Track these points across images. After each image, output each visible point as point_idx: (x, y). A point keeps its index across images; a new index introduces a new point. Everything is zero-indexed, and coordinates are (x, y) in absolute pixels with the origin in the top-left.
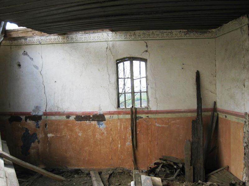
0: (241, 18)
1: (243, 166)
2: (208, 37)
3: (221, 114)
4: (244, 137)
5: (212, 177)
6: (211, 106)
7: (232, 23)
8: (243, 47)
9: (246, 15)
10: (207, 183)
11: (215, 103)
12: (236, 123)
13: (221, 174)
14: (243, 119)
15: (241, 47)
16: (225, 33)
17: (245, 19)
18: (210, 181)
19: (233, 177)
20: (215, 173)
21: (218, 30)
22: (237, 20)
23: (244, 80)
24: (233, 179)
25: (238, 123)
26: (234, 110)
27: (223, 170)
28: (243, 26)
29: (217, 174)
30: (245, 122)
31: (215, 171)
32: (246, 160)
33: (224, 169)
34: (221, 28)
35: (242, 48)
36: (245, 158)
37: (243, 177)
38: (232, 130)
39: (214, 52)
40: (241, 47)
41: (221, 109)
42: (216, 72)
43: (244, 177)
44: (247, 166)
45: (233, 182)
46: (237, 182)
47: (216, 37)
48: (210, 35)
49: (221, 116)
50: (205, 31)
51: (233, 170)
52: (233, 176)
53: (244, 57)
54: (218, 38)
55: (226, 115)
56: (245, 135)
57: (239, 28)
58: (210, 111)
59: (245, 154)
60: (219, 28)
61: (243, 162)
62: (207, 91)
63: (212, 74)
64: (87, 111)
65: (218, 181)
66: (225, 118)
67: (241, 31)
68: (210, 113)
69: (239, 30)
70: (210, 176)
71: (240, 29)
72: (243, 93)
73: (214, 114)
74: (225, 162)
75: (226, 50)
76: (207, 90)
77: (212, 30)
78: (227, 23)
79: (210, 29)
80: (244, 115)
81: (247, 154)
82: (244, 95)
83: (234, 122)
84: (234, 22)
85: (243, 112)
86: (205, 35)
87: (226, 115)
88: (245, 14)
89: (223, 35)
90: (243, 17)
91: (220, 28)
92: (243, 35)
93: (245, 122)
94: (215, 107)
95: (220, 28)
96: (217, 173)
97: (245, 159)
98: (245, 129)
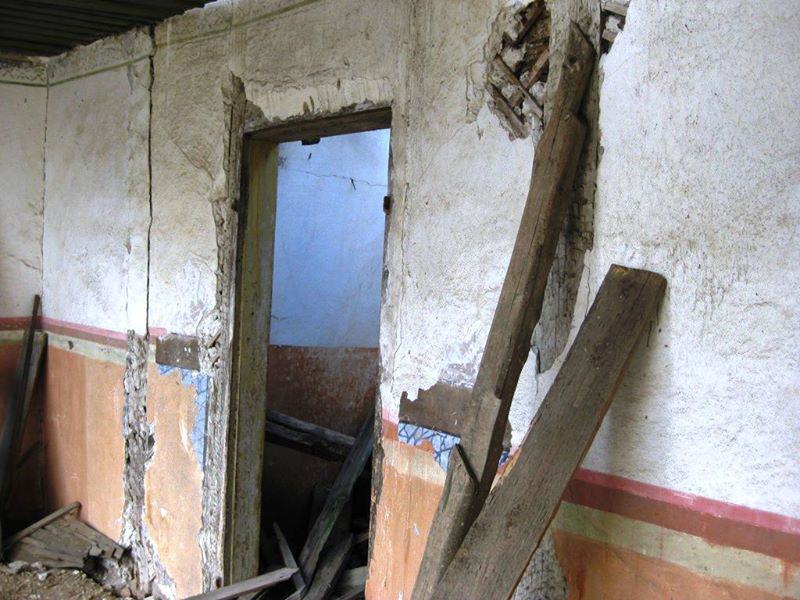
0: (132, 33)
1: (124, 498)
2: (26, 81)
3: (56, 335)
4: (126, 409)
5: (27, 544)
6: (23, 310)
7: (105, 47)
8: (132, 126)
9: (147, 28)
10: (10, 565)
11: (38, 300)
12: (101, 364)
13: (55, 531)
14: (123, 351)
15: (126, 124)
16: (79, 73)
17: (144, 40)
18: (20, 559)
19: (93, 537)
20: (36, 530)
21: (60, 61)
22: (120, 38)
23: (130, 230)
24: (94, 543)
25: (107, 365)
26: (95, 325)
27: (61, 517)
28: (137, 60)
29: (42, 531)
30: (130, 361)
31: (35, 522)
32: (131, 479)
33: (67, 512)
34: (70, 57)
35: (128, 129)
36: (128, 474)
37: (123, 532)
38: (89, 386)
39: (43, 133)
40: (126, 124)
41: (56, 321)
42: (43, 198)
43: (128, 532)
44: (134, 497)
45: (95, 552)
46: (106, 549)
47: (52, 85)
48: (31, 73)
49: (57, 342)
50: (18, 57)
51: (93, 515)
52: (94, 533)
53: (131, 157)
54: (58, 86)
55: (73, 339)
56: (127, 400)
57: (123, 65)
58: (20, 327)
59: (128, 461)
60: (63, 55)
61: (124, 485)
62: (12, 259)
63: (30, 205)
64: (525, 187)
65: (48, 554)
66: (68, 349)
67: (129, 75)
68: (19, 335)
69: (124, 71)
70: (22, 543)
71: (126, 67)
72: (124, 271)
73: (31, 337)
74: (70, 494)
75: (80, 130)
76: (12, 256)
77: (41, 58)
78: (89, 43)
79: (32, 56)
80: (124, 338)
81: (134, 459)
82: (126, 277)
83: (97, 362)
84: (111, 43)
85: (122, 331)
86: (16, 72)
87: (73, 339)
88: (144, 24)
89: (72, 79)
90: (138, 31)
91: (68, 56)
92: (132, 89)
93: (130, 361)
94: (38, 314)
95: (68, 56)
96: (43, 527)
97: (128, 476)
98: (129, 382)
